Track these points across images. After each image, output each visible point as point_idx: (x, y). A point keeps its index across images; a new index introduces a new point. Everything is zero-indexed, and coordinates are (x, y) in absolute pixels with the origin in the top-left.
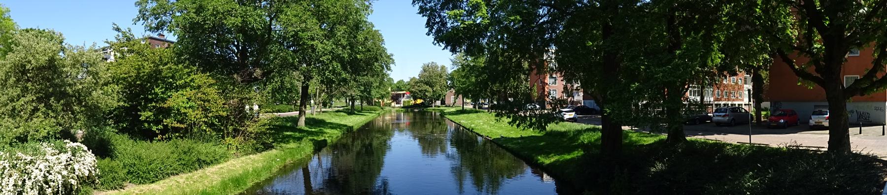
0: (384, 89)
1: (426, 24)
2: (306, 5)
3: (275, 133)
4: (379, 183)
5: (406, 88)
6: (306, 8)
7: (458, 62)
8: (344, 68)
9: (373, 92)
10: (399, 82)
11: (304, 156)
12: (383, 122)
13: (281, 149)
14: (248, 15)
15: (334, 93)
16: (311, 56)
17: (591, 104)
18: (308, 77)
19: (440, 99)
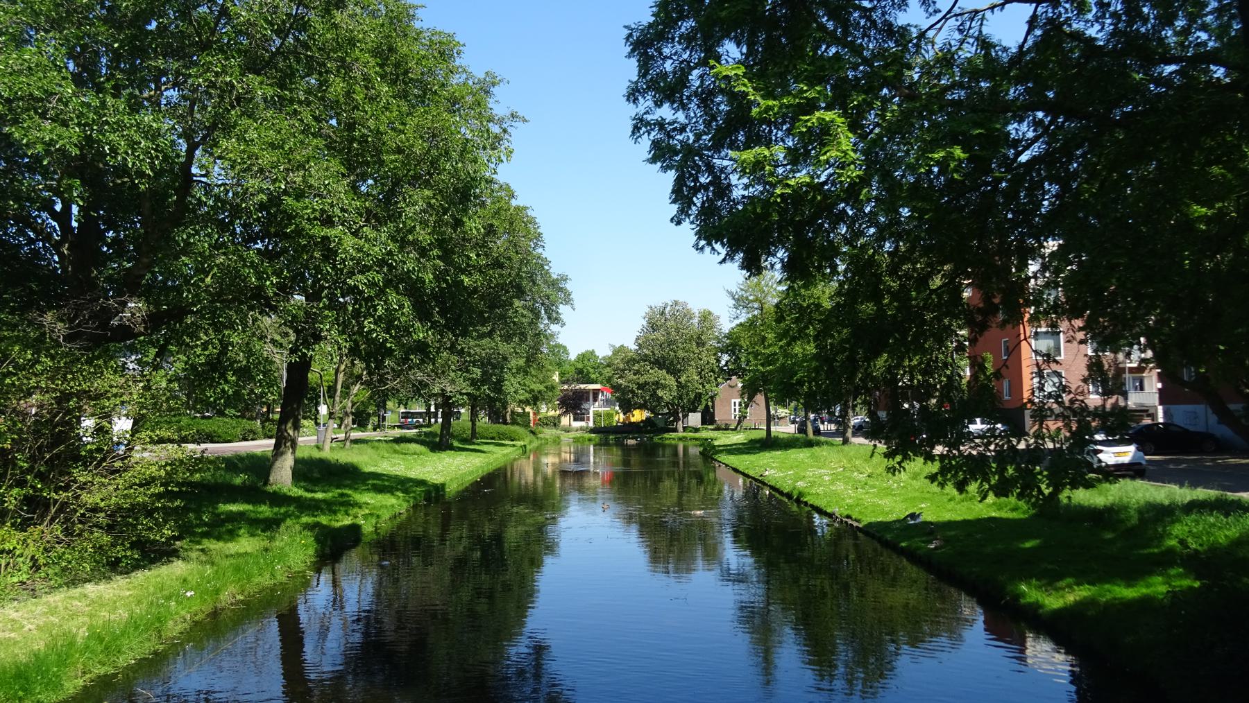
0: (540, 377)
1: (673, 192)
2: (309, 119)
3: (186, 509)
4: (519, 649)
5: (601, 374)
6: (308, 126)
7: (751, 298)
8: (422, 313)
9: (512, 384)
10: (583, 355)
11: (281, 577)
12: (536, 471)
13: (203, 558)
14: (107, 123)
15: (390, 385)
16: (318, 270)
17: (1195, 416)
18: (308, 336)
19: (701, 408)
